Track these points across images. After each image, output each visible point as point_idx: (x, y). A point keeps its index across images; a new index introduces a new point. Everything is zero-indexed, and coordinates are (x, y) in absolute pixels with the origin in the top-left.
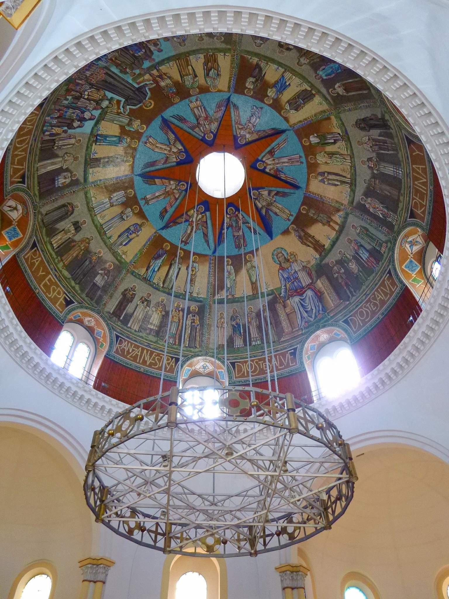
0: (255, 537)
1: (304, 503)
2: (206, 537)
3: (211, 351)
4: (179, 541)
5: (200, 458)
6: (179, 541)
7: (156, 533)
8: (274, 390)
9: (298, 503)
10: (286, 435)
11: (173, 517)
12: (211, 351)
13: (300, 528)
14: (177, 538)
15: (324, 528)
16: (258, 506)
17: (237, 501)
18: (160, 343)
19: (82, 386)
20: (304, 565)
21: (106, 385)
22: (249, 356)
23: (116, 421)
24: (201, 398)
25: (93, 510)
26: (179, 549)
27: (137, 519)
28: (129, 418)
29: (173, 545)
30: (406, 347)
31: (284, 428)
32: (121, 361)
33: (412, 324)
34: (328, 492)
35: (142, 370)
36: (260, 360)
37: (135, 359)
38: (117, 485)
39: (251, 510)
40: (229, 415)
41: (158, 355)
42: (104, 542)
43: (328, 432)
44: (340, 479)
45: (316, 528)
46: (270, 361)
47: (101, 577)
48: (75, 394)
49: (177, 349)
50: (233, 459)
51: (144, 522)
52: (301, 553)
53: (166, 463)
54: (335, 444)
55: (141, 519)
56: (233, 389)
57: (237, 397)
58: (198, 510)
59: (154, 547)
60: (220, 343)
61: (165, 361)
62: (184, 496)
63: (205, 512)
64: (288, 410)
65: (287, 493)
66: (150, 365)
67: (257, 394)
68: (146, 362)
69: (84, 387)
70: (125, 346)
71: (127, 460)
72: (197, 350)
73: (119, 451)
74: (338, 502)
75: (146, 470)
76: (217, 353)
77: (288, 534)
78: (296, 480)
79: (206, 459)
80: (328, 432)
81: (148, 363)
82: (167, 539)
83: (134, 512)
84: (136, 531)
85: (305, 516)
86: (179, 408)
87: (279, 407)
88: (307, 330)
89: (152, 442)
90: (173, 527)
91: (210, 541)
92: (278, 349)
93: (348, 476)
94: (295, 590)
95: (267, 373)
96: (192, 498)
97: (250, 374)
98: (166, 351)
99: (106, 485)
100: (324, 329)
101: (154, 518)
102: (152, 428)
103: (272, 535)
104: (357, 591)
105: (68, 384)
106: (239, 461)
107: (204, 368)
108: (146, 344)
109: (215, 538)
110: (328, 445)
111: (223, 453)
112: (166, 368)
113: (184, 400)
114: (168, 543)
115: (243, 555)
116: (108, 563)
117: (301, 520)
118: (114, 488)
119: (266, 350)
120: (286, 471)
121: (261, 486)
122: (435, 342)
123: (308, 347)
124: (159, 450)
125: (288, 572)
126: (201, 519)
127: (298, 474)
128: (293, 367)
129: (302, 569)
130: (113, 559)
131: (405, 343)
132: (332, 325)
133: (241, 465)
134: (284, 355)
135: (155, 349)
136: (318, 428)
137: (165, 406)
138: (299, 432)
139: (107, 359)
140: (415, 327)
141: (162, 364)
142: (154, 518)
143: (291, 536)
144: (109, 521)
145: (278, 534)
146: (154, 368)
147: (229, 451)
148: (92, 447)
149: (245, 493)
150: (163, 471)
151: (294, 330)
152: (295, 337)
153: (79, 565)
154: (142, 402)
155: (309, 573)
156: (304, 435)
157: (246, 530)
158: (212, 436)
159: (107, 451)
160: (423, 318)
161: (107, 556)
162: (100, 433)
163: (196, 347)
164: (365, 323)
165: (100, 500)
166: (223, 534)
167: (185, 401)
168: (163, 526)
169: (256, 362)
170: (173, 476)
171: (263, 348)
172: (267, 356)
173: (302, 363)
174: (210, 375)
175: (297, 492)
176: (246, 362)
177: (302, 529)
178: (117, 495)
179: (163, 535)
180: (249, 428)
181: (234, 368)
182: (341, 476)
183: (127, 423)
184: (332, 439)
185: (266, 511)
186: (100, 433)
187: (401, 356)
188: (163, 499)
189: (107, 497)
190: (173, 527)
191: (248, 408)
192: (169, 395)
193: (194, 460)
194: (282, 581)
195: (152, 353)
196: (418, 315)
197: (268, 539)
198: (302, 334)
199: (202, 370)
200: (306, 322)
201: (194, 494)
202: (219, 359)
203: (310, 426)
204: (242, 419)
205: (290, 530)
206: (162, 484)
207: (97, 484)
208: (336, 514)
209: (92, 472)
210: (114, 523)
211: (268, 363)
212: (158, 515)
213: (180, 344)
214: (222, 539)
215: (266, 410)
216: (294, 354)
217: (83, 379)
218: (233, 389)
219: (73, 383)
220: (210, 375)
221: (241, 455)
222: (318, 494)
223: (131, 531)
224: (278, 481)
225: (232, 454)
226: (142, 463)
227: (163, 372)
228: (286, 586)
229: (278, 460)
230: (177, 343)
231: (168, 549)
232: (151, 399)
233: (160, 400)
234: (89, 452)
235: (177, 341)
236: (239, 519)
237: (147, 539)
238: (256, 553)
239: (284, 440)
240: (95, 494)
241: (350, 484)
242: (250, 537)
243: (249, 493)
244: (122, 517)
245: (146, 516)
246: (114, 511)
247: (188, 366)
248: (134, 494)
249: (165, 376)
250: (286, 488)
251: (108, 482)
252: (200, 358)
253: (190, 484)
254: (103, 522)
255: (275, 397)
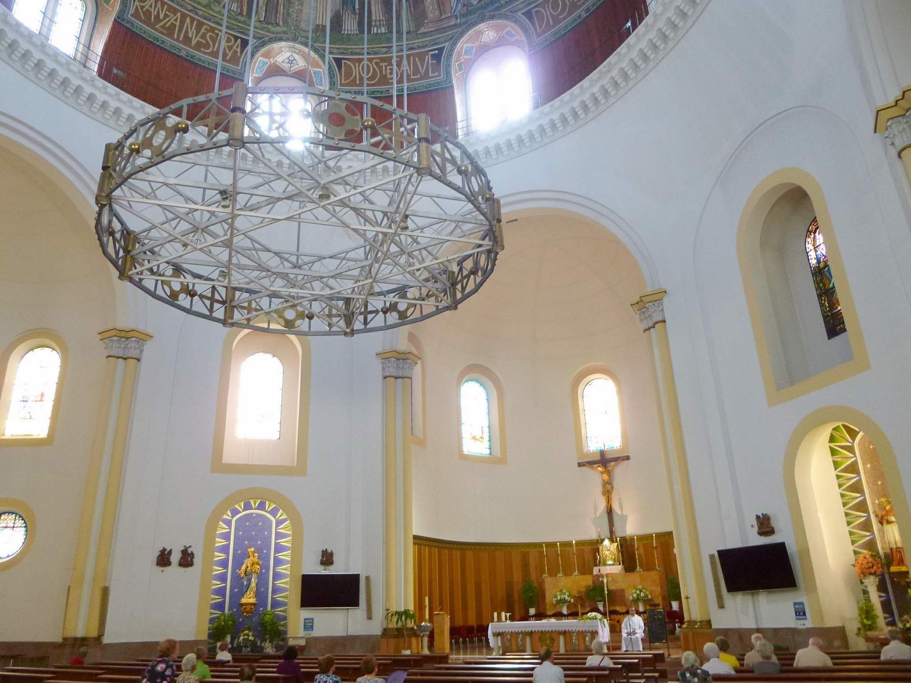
0: (353, 313)
1: (426, 275)
2: (285, 309)
3: (303, 34)
4: (246, 312)
5: (279, 199)
6: (246, 312)
7: (212, 300)
8: (400, 105)
9: (417, 274)
10: (411, 176)
11: (237, 279)
12: (303, 34)
13: (415, 305)
14: (243, 308)
15: (447, 308)
16: (361, 273)
17: (332, 264)
18: (215, 8)
19: (75, 69)
20: (415, 352)
21: (121, 74)
22: (365, 51)
23: (142, 130)
24: (284, 106)
25: (115, 264)
26: (246, 322)
27: (182, 279)
28: (163, 127)
29: (237, 316)
30: (609, 71)
31: (411, 166)
32: (145, 33)
33: (628, 33)
34: (460, 263)
35: (183, 54)
36: (383, 60)
37: (170, 31)
38: (149, 230)
39: (351, 278)
40: (327, 137)
41: (212, 30)
42: (134, 307)
43: (473, 179)
44: (480, 246)
45: (437, 307)
46: (399, 65)
47: (134, 353)
48: (65, 82)
49: (244, 22)
50: (329, 204)
51: (194, 284)
52: (412, 337)
53: (227, 203)
54: (480, 198)
55: (189, 279)
56: (337, 98)
57: (342, 109)
58: (274, 274)
59: (210, 318)
60: (319, 22)
61: (223, 44)
62: (254, 252)
63: (284, 276)
64: (420, 140)
65: (403, 260)
66: (198, 46)
67: (374, 109)
68: (190, 40)
69: (80, 72)
70: (151, 6)
71: (163, 192)
72: (278, 29)
73: (150, 178)
74: (472, 276)
75: (196, 210)
76: (313, 39)
77: (399, 312)
78: (418, 243)
79: (289, 202)
80: (473, 179)
81: (194, 42)
82: (229, 308)
83: (178, 270)
84: (182, 296)
85: (424, 291)
86: (248, 118)
87: (405, 134)
88: (464, 20)
89: (203, 169)
90: (238, 293)
91: (290, 314)
92: (414, 46)
93: (491, 243)
94: (400, 380)
95: (392, 84)
96: (264, 256)
97: (366, 82)
98: (225, 24)
99: (131, 229)
100: (491, 22)
101: (208, 279)
102: (203, 145)
103: (377, 312)
104: (477, 385)
105: (50, 65)
106: (337, 209)
107: (291, 62)
108: (189, 7)
109: (297, 311)
110: (471, 198)
111: (314, 195)
112: (225, 55)
113: (256, 106)
114: (229, 312)
115: (336, 334)
116: (142, 336)
117: (417, 296)
118: (145, 234)
119: (394, 44)
120: (407, 228)
121: (368, 248)
122: (654, 67)
123: (462, 48)
124: (215, 181)
125: (393, 359)
126: (278, 285)
127: (422, 234)
128: (434, 78)
129: (410, 356)
130: (150, 331)
131: (610, 64)
132: (505, 17)
133: (341, 214)
134: (422, 56)
135: (206, 18)
136: (460, 172)
137: (225, 113)
138: (432, 174)
139: (118, 25)
140: (631, 39)
141: (219, 47)
142: (208, 279)
143: (402, 315)
144: (141, 280)
145: (385, 311)
146: (205, 53)
147: (325, 192)
148: (105, 168)
149: (343, 255)
150: (221, 214)
151: (443, 17)
152: (444, 30)
153: (100, 337)
154: (185, 102)
155: (419, 362)
156: (438, 179)
157: (341, 303)
158: (299, 167)
159: (130, 176)
160: (647, 26)
161: (141, 327)
162: (116, 149)
163: (278, 25)
164: (557, 21)
165: (125, 252)
166: (308, 306)
167: (258, 107)
168: (223, 291)
169: (377, 64)
170: (239, 223)
171: (389, 40)
172: (395, 54)
173: (448, 74)
174: (300, 75)
175: (418, 259)
176: (361, 60)
177: (418, 307)
178: (149, 244)
179: (223, 302)
180: (354, 161)
181: (340, 67)
182: (481, 242)
183: (162, 134)
184: (477, 189)
185: (371, 280)
186: (116, 149)
187: (599, 84)
188: (223, 255)
189: (134, 246)
190: (238, 293)
191: (359, 129)
192: (231, 95)
193: (271, 201)
194: (383, 369)
195: (200, 25)
196: (641, 19)
197: (370, 317)
198: (455, 26)
199: (286, 66)
200: (464, 5)
201: (269, 251)
202: (316, 51)
203: (449, 167)
204: (347, 145)
205: (402, 307)
206: (221, 233)
207: (116, 226)
208: (466, 292)
209: (107, 207)
210: (149, 283)
211: (395, 68)
212: (215, 276)
213: (250, 17)
214: (307, 312)
215: (386, 136)
216: (437, 57)
217: (78, 58)
218: (337, 98)
219: (60, 64)
220: (300, 75)
221: (341, 200)
222: (447, 264)
223: (174, 295)
224: (392, 242)
225: (328, 197)
226: (188, 199)
227: (220, 62)
228: (388, 374)
229: (396, 212)
230: (245, 13)
231: (230, 321)
232: (201, 98)
233: (216, 102)
234: (98, 179)
235: (245, 8)
236: (332, 289)
237: (199, 306)
238: (353, 332)
239: (408, 184)
240: (115, 240)
241: (492, 254)
242: (346, 313)
243: (350, 255)
244: (160, 275)
245: (196, 276)
246: (147, 265)
247: (263, 56)
248: (178, 246)
249: (223, 68)
250: (402, 252)
251: (135, 225)
252: (283, 44)
253: (262, 236)
254: (131, 279)
255: (402, 117)
